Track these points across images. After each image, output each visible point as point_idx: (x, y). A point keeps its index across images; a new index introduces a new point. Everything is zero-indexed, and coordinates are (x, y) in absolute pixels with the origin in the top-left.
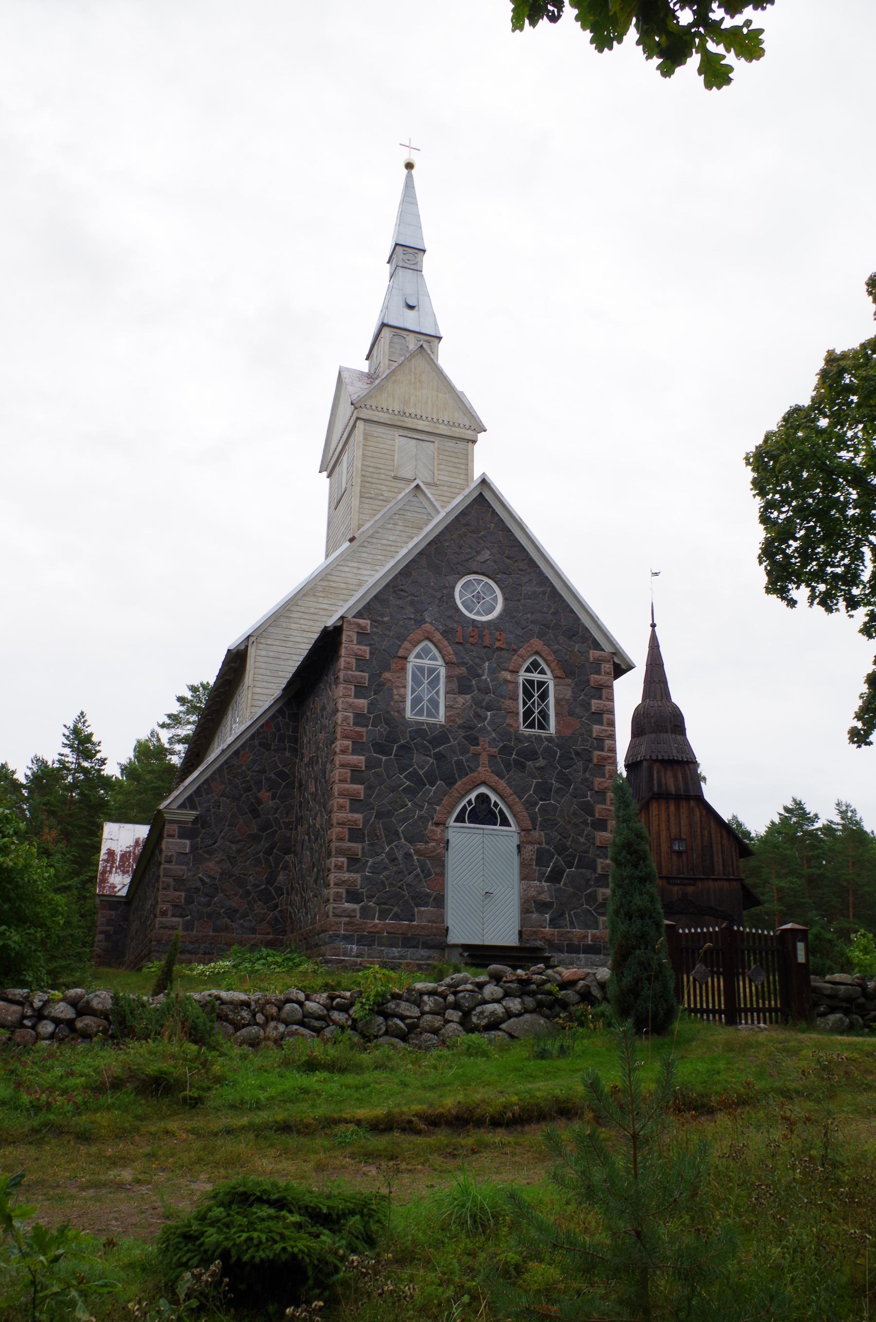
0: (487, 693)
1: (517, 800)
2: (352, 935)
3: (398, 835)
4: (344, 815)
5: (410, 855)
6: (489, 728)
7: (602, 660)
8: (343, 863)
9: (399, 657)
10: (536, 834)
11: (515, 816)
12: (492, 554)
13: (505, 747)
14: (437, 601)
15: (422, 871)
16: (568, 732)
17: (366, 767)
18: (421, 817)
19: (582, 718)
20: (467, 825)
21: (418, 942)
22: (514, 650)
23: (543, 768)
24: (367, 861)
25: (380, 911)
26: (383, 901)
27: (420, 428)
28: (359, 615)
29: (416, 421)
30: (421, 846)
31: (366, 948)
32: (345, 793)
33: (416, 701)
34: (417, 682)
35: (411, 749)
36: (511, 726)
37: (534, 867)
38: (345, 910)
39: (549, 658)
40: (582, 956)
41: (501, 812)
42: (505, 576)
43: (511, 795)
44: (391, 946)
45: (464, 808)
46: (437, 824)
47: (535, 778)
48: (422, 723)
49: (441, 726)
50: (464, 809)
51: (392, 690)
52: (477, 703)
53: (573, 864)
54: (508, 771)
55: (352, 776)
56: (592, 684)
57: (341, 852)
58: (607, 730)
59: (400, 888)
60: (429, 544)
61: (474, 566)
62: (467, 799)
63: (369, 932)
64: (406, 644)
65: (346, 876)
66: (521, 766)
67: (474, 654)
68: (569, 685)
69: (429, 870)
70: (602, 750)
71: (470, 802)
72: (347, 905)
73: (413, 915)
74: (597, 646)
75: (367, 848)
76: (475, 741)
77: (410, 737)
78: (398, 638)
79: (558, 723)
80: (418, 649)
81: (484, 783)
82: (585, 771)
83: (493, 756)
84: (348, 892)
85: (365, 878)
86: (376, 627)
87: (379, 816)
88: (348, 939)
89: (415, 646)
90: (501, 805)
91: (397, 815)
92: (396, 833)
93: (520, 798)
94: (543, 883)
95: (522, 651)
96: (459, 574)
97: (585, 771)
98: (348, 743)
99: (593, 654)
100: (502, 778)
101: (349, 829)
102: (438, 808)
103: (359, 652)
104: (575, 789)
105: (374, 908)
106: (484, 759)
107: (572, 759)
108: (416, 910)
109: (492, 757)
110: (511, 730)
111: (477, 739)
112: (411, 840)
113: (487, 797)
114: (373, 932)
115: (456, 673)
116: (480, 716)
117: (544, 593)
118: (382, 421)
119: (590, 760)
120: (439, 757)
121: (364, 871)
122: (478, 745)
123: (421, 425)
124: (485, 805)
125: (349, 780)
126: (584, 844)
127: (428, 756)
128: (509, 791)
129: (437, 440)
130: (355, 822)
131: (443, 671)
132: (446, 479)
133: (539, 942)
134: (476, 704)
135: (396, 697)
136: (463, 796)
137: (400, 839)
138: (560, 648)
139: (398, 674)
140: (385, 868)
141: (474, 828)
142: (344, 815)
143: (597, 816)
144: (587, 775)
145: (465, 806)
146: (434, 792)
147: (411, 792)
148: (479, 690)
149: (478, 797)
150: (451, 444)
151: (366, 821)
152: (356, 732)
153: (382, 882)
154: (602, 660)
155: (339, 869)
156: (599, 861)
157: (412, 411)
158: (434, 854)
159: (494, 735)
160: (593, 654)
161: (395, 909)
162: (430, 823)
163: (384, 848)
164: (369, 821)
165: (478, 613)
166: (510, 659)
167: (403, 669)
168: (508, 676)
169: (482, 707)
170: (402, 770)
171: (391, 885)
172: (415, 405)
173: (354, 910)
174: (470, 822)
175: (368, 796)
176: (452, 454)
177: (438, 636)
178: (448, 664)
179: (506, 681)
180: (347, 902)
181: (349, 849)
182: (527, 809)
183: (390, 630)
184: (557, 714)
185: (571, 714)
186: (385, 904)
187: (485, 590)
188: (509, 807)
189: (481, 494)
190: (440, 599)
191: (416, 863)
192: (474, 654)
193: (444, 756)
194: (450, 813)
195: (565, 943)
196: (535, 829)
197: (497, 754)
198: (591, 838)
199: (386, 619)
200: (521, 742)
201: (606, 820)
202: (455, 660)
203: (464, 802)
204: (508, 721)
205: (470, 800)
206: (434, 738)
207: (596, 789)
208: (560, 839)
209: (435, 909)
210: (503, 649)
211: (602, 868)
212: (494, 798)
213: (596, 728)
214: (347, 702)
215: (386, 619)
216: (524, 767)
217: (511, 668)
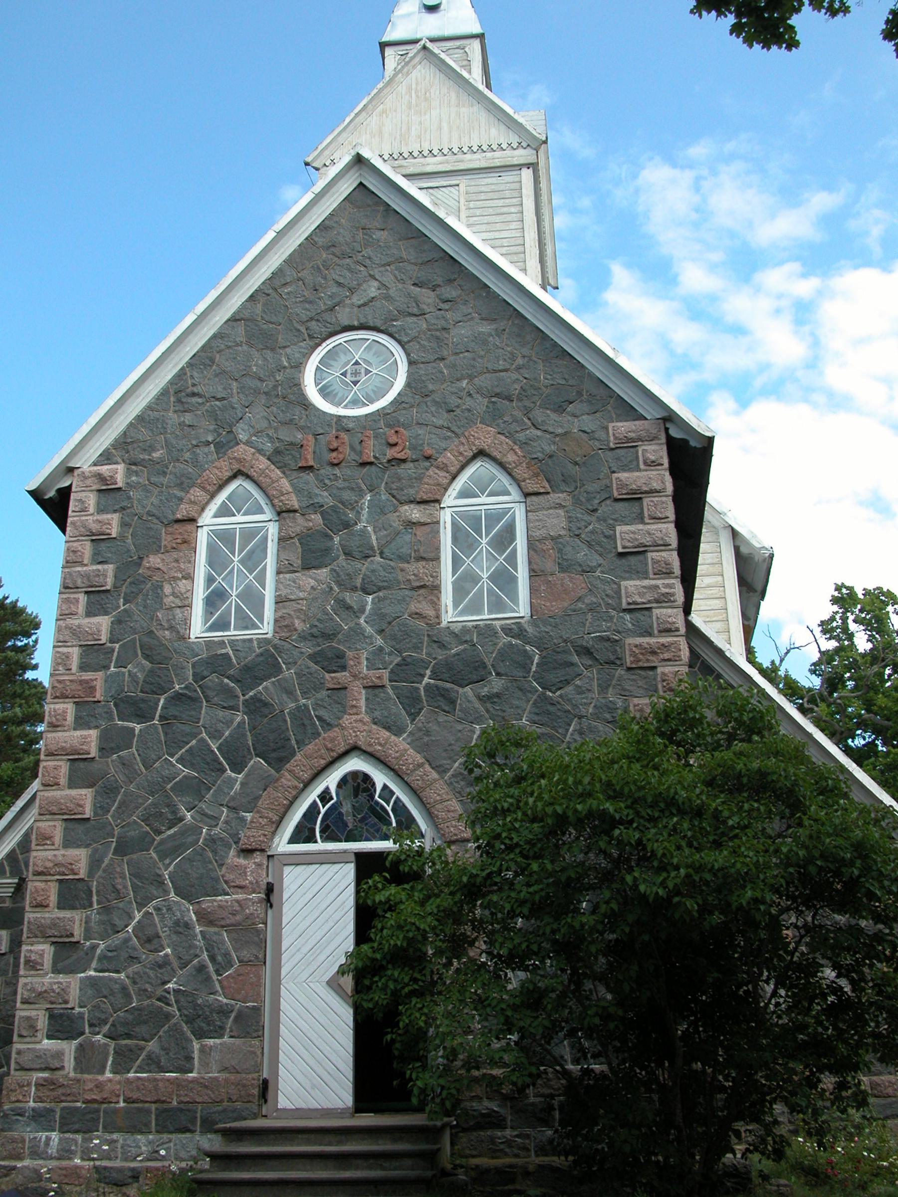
1: (435, 775)
3: (162, 883)
4: (50, 854)
5: (188, 926)
6: (369, 629)
9: (178, 521)
13: (404, 663)
15: (212, 958)
16: (556, 607)
17: (101, 749)
18: (212, 841)
19: (592, 570)
20: (321, 846)
21: (193, 1120)
22: (428, 458)
23: (498, 695)
24: (94, 947)
26: (121, 1030)
27: (429, 169)
31: (79, 1137)
32: (54, 809)
33: (215, 599)
34: (216, 561)
35: (194, 700)
36: (419, 615)
39: (510, 458)
41: (399, 807)
44: (134, 1129)
45: (313, 808)
46: (247, 852)
47: (479, 720)
48: (222, 644)
49: (267, 641)
50: (313, 811)
51: (161, 587)
52: (344, 582)
54: (413, 716)
63: (86, 1102)
64: (197, 493)
67: (340, 484)
68: (561, 506)
69: (227, 955)
71: (325, 796)
73: (189, 1059)
77: (195, 675)
79: (533, 590)
81: (354, 750)
82: (604, 689)
83: (375, 687)
84: (53, 1017)
86: (136, 473)
87: (122, 849)
88: (41, 1118)
89: (213, 496)
90: (399, 792)
91: (162, 842)
92: (159, 882)
97: (604, 689)
100: (398, 732)
101: (60, 881)
102: (248, 816)
108: (196, 1045)
110: (421, 624)
111: (341, 656)
113: (367, 778)
116: (349, 608)
122: (344, 668)
124: (363, 797)
125: (63, 781)
129: (463, 182)
131: (273, 530)
133: (486, 1103)
135: (169, 600)
136: (308, 784)
137: (166, 892)
139: (175, 555)
140: (133, 959)
142: (50, 854)
144: (611, 695)
145: (314, 805)
146: (242, 784)
149: (343, 782)
150: (491, 180)
151: (95, 863)
152: (81, 682)
153: (124, 989)
155: (34, 968)
158: (238, 918)
161: (152, 1046)
164: (99, 861)
165: (355, 403)
166: (419, 478)
167: (189, 544)
169: (354, 589)
170: (173, 745)
171: (142, 992)
172: (420, 137)
173: (59, 1055)
175: (101, 808)
176: (491, 196)
178: (282, 513)
180: (49, 1037)
183: (165, 474)
186: (128, 1036)
188: (415, 792)
191: (200, 942)
194: (278, 824)
199: (156, 455)
200: (442, 646)
203: (313, 795)
205: (327, 791)
206: (247, 669)
210: (404, 461)
212: (380, 778)
215: (156, 455)
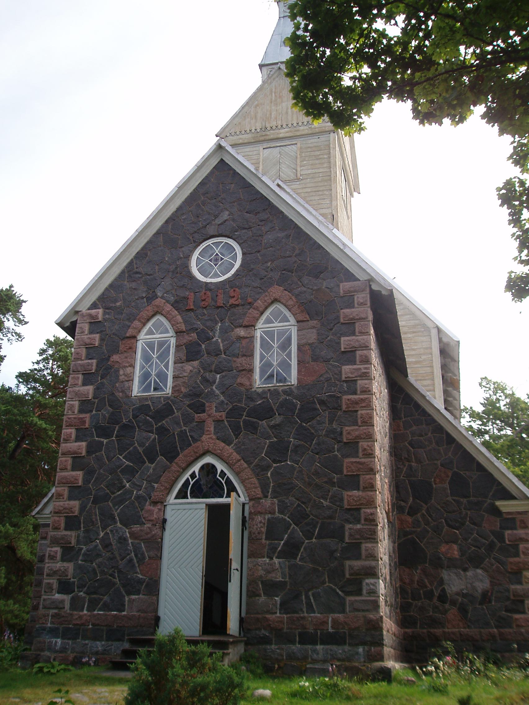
0: (217, 355)
1: (245, 465)
2: (57, 629)
5: (125, 539)
6: (217, 392)
7: (355, 291)
8: (56, 552)
9: (128, 337)
10: (267, 503)
11: (243, 482)
12: (231, 214)
14: (170, 274)
15: (136, 555)
18: (138, 497)
20: (190, 500)
22: (250, 303)
25: (90, 601)
27: (281, 136)
28: (94, 306)
29: (277, 131)
30: (136, 528)
31: (70, 642)
32: (64, 481)
33: (146, 376)
36: (241, 384)
37: (264, 541)
38: (53, 602)
40: (319, 647)
42: (244, 231)
43: (239, 460)
44: (95, 639)
46: (155, 503)
47: (269, 438)
49: (168, 398)
51: (119, 371)
52: (205, 367)
53: (313, 534)
54: (237, 436)
55: (73, 462)
56: (342, 320)
57: (55, 541)
58: (360, 369)
59: (111, 575)
60: (167, 222)
61: (211, 230)
62: (190, 472)
63: (74, 625)
64: (136, 323)
65: (59, 565)
66: (252, 428)
67: (206, 317)
68: (314, 327)
69: (143, 554)
70: (355, 393)
71: (193, 476)
72: (57, 596)
74: (350, 276)
75: (82, 534)
76: (200, 408)
78: (128, 320)
80: (149, 325)
82: (331, 422)
83: (218, 421)
84: (60, 582)
85: (78, 568)
86: (108, 314)
88: (54, 632)
91: (115, 497)
93: (249, 463)
94: (276, 560)
95: (259, 303)
96: (195, 242)
97: (331, 422)
98: (73, 431)
99: (345, 286)
101: (66, 517)
102: (156, 485)
103: (88, 341)
104: (318, 444)
105: (85, 598)
106: (210, 426)
107: (316, 409)
108: (127, 599)
109: (218, 422)
110: (243, 389)
111: (203, 405)
112: (126, 524)
113: (213, 467)
114: (77, 624)
115: (185, 341)
116: (208, 381)
117: (288, 236)
118: (246, 141)
119: (339, 408)
120: (162, 431)
121: (77, 560)
122: (204, 411)
123: (283, 133)
126: (329, 508)
127: (149, 432)
128: (236, 456)
130: (71, 510)
131: (173, 341)
132: (309, 172)
133: (263, 631)
134: (204, 369)
135: (122, 378)
136: (185, 469)
137: (116, 523)
138: (305, 289)
139: (125, 354)
140: (99, 555)
141: (196, 503)
142: (61, 503)
143: (345, 472)
145: (187, 481)
146: (154, 469)
147: (130, 472)
148: (208, 353)
149: (202, 468)
151: (82, 508)
153: (94, 570)
154: (355, 291)
156: (348, 526)
157: (274, 124)
158: (149, 536)
159: (222, 398)
160: (345, 286)
161: (106, 598)
162: (148, 503)
163: (98, 534)
164: (85, 507)
166: (245, 314)
167: (132, 349)
168: (242, 332)
171: (102, 572)
172: (276, 118)
173: (63, 601)
174: (192, 497)
175: (86, 481)
177: (168, 307)
178: (178, 333)
179: (240, 338)
180: (59, 593)
181: (63, 538)
182: (257, 475)
184: (300, 362)
185: (315, 359)
186: (95, 593)
187: (223, 251)
188: (237, 474)
189: (222, 160)
190: (173, 272)
191: (130, 547)
192: (206, 317)
193: (167, 430)
194: (169, 490)
195: (297, 632)
196: (266, 497)
197: (224, 417)
198: (337, 500)
199: (118, 304)
201: (358, 475)
202: (183, 328)
203: (187, 475)
204: (239, 380)
207: (345, 440)
208: (299, 505)
209: (146, 597)
210: (238, 305)
211: (351, 535)
212: (220, 467)
213: (347, 369)
214: (73, 391)
215: (118, 304)
216: (256, 428)
217: (246, 323)
